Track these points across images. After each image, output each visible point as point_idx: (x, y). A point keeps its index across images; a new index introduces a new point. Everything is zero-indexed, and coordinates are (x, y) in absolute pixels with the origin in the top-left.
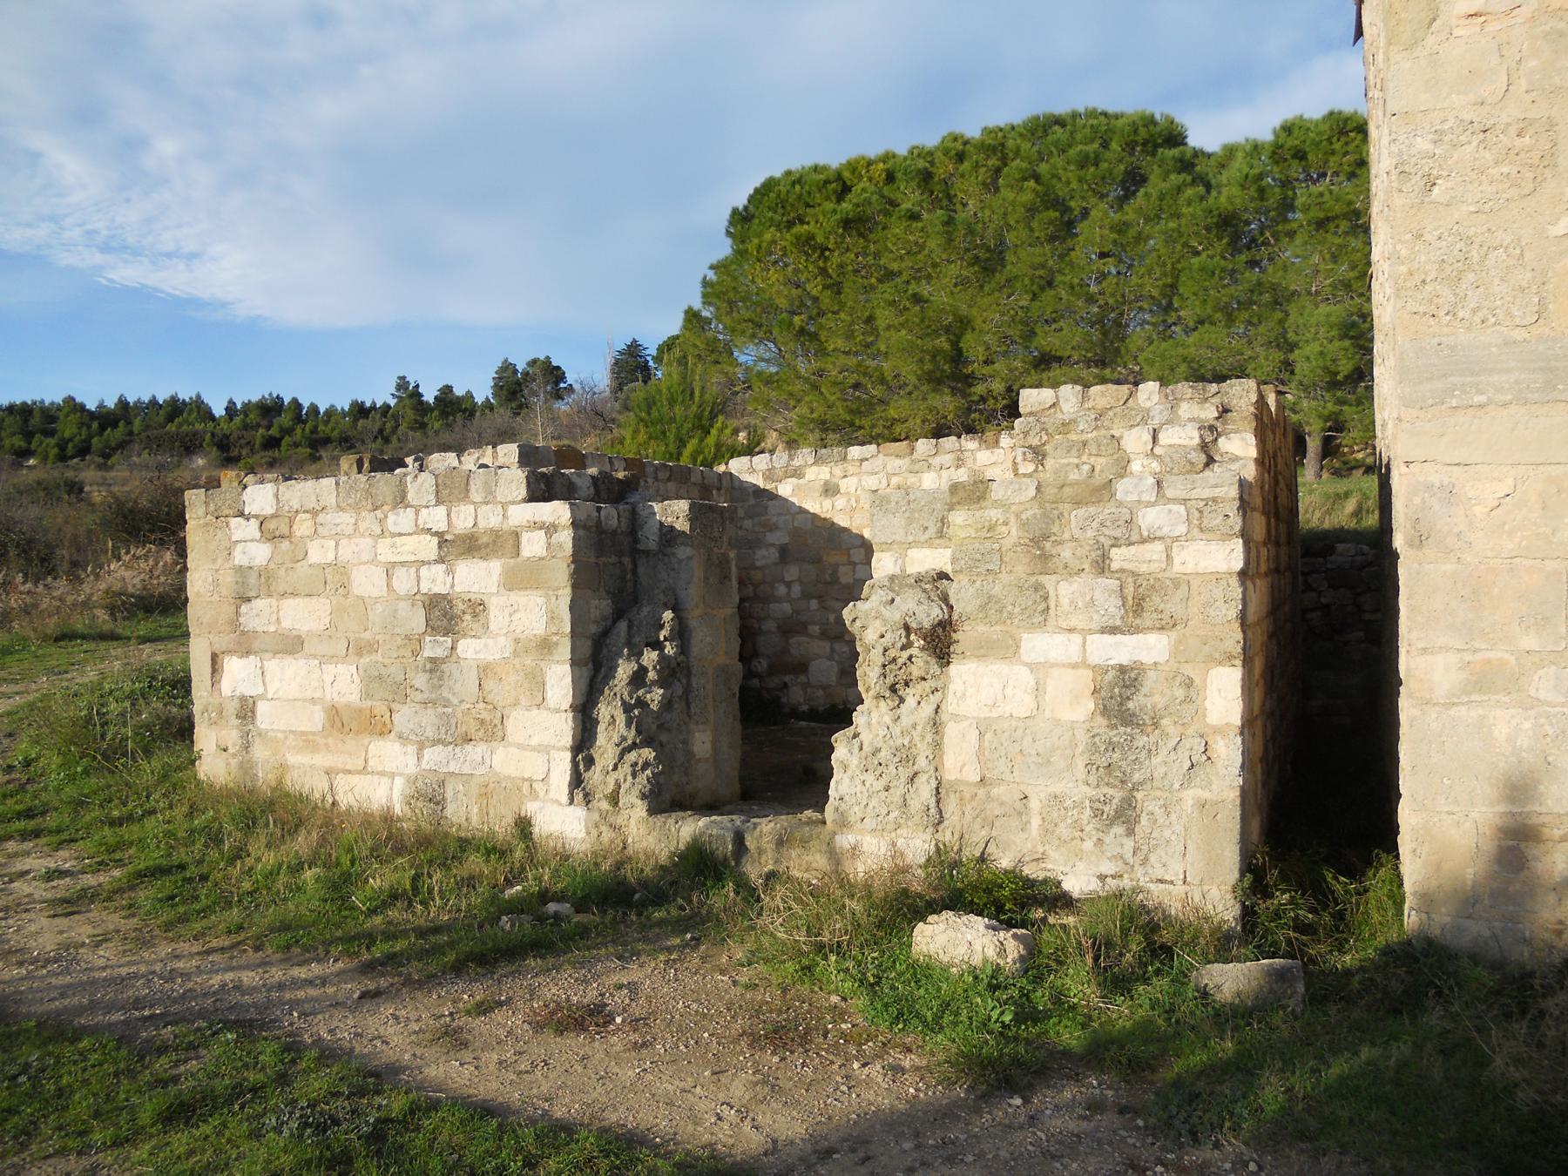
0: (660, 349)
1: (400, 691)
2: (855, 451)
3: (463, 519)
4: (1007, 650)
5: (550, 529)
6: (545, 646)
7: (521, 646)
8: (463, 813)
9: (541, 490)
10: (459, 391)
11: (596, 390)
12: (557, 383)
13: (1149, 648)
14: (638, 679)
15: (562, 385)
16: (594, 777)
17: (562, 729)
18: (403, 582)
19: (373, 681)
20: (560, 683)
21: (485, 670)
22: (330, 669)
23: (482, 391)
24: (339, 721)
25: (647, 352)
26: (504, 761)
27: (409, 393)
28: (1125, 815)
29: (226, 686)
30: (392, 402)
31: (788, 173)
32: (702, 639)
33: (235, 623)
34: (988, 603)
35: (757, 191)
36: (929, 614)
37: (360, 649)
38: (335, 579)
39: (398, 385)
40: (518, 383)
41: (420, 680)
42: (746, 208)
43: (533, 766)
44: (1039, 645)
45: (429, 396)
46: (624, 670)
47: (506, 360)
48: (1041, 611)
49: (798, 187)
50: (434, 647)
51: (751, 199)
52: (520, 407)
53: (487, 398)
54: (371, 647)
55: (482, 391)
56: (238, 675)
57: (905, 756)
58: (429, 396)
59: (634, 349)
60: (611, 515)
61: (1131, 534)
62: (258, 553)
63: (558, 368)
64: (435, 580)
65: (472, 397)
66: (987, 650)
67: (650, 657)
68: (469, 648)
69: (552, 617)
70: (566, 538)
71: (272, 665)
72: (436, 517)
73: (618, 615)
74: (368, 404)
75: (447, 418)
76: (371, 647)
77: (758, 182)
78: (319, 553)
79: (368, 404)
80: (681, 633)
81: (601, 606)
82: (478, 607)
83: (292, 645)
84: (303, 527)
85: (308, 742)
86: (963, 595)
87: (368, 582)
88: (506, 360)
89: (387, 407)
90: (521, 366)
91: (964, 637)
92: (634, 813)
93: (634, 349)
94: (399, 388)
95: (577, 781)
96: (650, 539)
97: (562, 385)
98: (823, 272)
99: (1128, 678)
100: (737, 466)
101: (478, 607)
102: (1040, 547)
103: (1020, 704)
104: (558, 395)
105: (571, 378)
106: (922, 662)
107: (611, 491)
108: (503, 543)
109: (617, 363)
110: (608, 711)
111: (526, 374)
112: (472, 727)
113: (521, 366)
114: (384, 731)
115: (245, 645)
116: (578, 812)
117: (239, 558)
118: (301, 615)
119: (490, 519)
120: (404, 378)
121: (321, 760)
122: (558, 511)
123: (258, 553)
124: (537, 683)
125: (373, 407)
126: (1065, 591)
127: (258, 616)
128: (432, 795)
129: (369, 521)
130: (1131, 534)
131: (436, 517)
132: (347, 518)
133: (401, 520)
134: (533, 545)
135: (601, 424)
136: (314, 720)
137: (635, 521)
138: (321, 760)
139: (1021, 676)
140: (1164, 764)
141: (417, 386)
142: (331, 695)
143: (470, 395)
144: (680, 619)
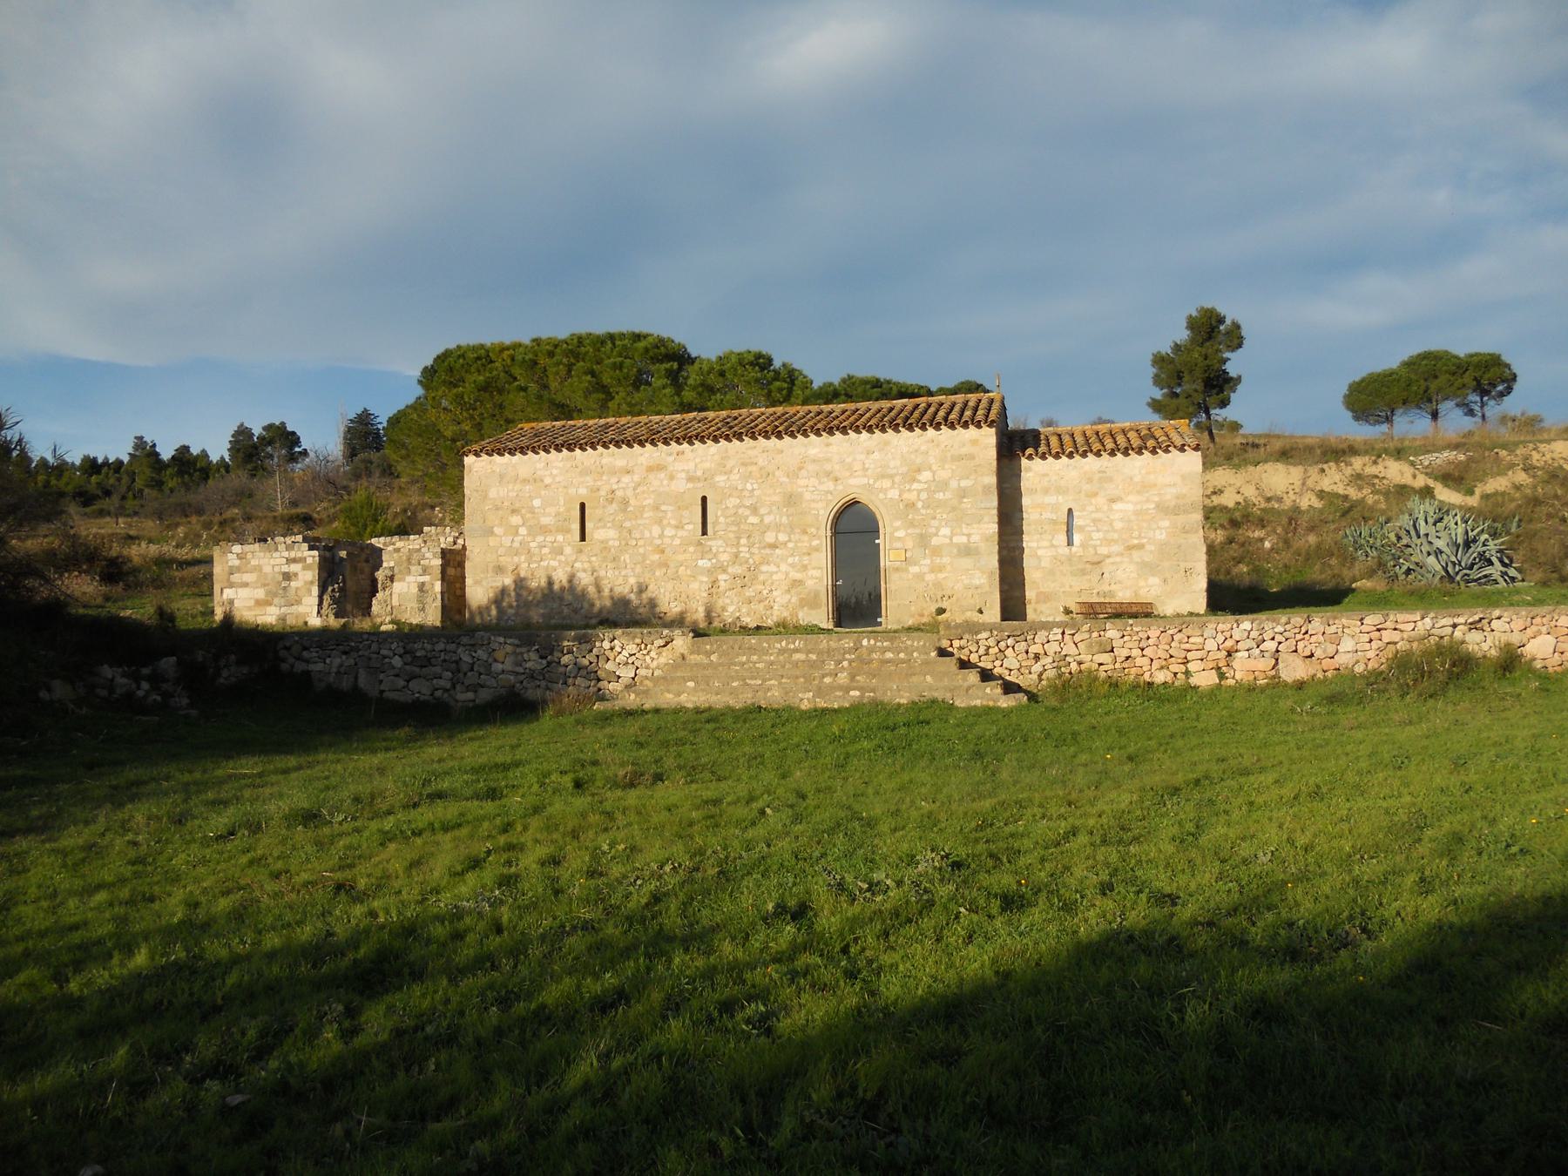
0: (390, 420)
1: (275, 595)
2: (412, 537)
3: (293, 554)
4: (403, 580)
5: (314, 557)
6: (312, 583)
7: (306, 583)
8: (291, 621)
9: (311, 548)
10: (195, 451)
11: (330, 458)
12: (291, 448)
13: (426, 578)
14: (333, 590)
15: (297, 449)
16: (322, 612)
17: (316, 601)
18: (277, 569)
19: (268, 593)
20: (315, 590)
21: (297, 589)
22: (256, 591)
23: (218, 450)
24: (259, 603)
25: (378, 420)
26: (301, 609)
27: (145, 452)
28: (423, 609)
29: (225, 596)
30: (126, 459)
31: (459, 347)
32: (349, 583)
33: (228, 580)
34: (400, 571)
35: (438, 357)
36: (390, 574)
37: (264, 585)
38: (259, 568)
39: (136, 444)
40: (255, 447)
41: (281, 592)
42: (432, 366)
43: (308, 610)
44: (409, 579)
45: (166, 453)
46: (330, 589)
47: (242, 425)
48: (409, 572)
49: (461, 361)
50: (284, 584)
51: (435, 360)
52: (255, 469)
53: (222, 458)
54: (268, 585)
55: (218, 450)
56: (229, 593)
57: (385, 601)
58: (166, 453)
59: (364, 419)
60: (328, 554)
61: (424, 558)
62: (237, 563)
63: (293, 433)
64: (285, 569)
65: (207, 456)
66: (400, 580)
67: (336, 586)
68: (293, 584)
69: (314, 576)
70: (317, 559)
71: (240, 590)
72: (286, 554)
73: (329, 576)
74: (100, 461)
75: (182, 477)
76: (268, 585)
77: (440, 350)
78: (254, 562)
79: (100, 461)
80: (344, 581)
81: (325, 575)
82: (296, 575)
83: (246, 585)
84: (249, 556)
85: (250, 608)
86: (396, 570)
87: (267, 569)
88: (242, 425)
89: (119, 463)
90: (257, 431)
91: (396, 577)
92: (332, 619)
93: (364, 419)
94: (136, 447)
95: (319, 612)
96: (337, 559)
97: (297, 449)
98: (472, 417)
99: (423, 584)
100: (374, 541)
101: (296, 575)
102: (409, 560)
103: (406, 590)
104: (293, 458)
105: (306, 443)
106: (389, 583)
107: (327, 548)
108: (303, 560)
109: (349, 430)
110: (325, 604)
111: (261, 438)
112: (293, 602)
113: (257, 431)
114: (271, 605)
115: (231, 585)
116: (319, 619)
117: (230, 564)
118: (247, 577)
119: (299, 555)
120: (142, 438)
121: (253, 613)
122: (316, 553)
123: (237, 563)
124: (310, 591)
125: (106, 463)
126: (413, 568)
127: (236, 578)
128: (283, 619)
129: (268, 554)
130: (424, 558)
131: (286, 554)
132: (262, 554)
133: (276, 555)
134: (309, 560)
135: (333, 490)
136: (252, 603)
137: (333, 557)
138: (253, 613)
139: (405, 584)
140: (429, 600)
141: (154, 445)
142: (257, 596)
143: (204, 454)
144: (343, 578)
